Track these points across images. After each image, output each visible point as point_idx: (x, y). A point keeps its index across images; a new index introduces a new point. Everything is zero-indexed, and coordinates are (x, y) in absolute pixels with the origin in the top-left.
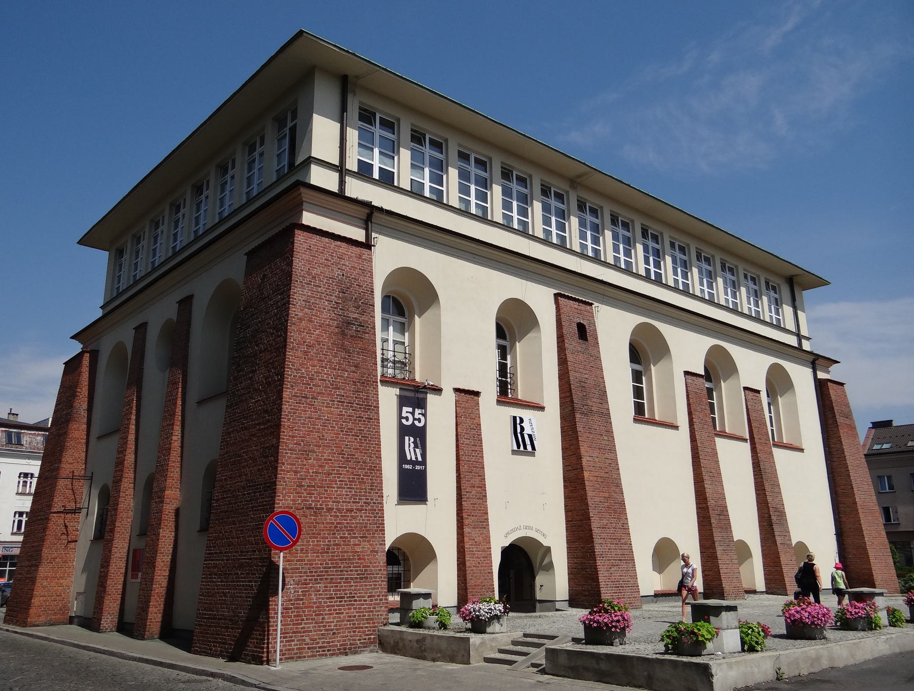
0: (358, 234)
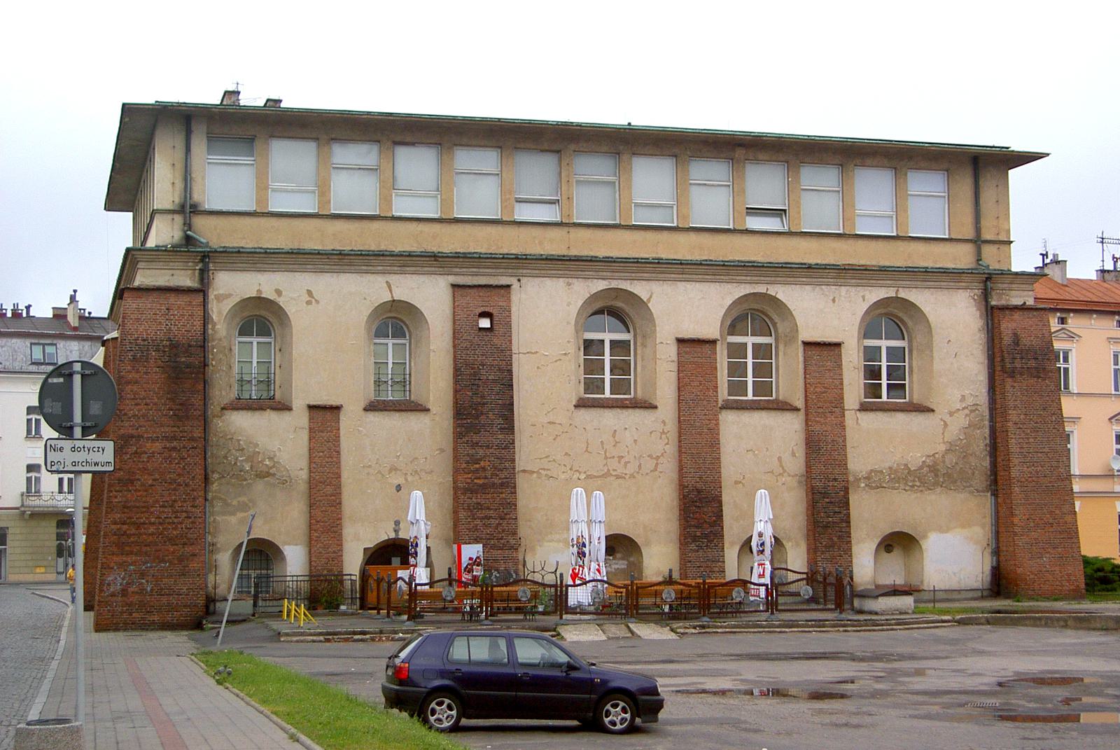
0: (185, 278)
